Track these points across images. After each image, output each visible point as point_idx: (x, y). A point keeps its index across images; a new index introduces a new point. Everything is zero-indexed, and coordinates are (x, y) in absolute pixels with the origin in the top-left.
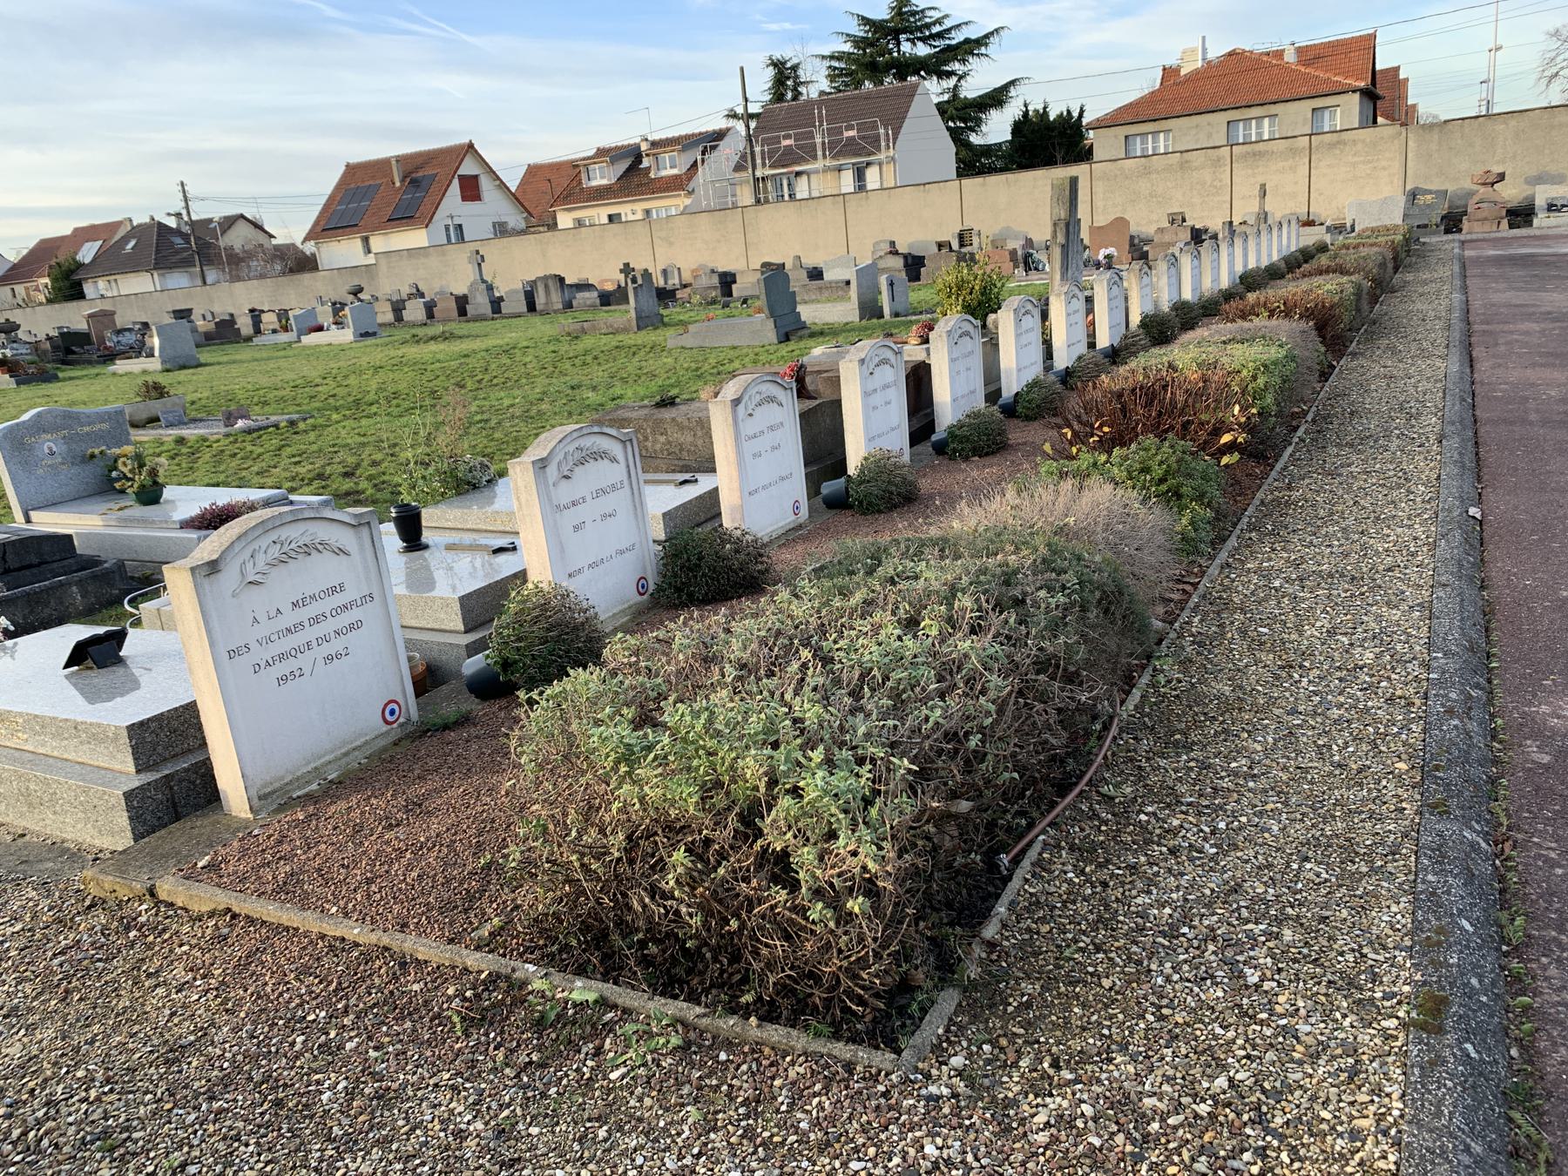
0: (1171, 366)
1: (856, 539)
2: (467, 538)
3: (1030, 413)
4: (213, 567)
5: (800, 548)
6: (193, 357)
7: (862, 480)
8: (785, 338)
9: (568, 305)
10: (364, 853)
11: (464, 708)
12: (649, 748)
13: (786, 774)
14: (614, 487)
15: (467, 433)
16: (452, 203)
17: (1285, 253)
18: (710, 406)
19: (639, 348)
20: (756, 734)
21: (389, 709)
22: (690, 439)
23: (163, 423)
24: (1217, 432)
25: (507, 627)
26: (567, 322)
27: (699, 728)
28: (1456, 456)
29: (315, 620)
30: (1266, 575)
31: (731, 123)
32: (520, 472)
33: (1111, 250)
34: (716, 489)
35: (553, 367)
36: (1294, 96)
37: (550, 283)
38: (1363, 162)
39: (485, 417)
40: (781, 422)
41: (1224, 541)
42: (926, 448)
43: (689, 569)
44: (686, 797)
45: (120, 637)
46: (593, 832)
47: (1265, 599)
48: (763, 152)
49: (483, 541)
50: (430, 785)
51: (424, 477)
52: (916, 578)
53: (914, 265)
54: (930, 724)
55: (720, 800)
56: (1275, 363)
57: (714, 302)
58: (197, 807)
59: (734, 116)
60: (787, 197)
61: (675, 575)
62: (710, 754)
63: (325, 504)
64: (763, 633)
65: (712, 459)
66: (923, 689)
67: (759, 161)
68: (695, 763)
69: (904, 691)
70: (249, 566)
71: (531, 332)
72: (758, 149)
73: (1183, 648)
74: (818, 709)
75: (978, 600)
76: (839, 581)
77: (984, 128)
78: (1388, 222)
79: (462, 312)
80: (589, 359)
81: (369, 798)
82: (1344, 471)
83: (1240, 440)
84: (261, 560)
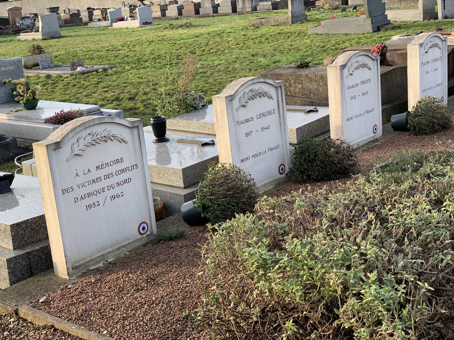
1: (409, 150)
2: (190, 137)
4: (57, 145)
5: (375, 153)
7: (417, 114)
8: (377, 29)
9: (254, 9)
10: (123, 303)
11: (181, 229)
12: (277, 262)
13: (354, 285)
14: (269, 113)
15: (194, 79)
18: (328, 69)
19: (291, 33)
20: (338, 260)
21: (142, 227)
22: (315, 86)
23: (40, 67)
25: (206, 187)
26: (253, 18)
27: (304, 253)
29: (107, 177)
32: (218, 103)
34: (328, 116)
35: (243, 44)
39: (204, 70)
40: (370, 78)
43: (309, 161)
44: (296, 293)
45: (10, 178)
46: (243, 305)
49: (199, 139)
50: (160, 269)
51: (169, 102)
52: (444, 175)
54: (444, 264)
55: (314, 295)
57: (337, 8)
58: (42, 270)
61: (301, 164)
62: (311, 269)
63: (118, 115)
64: (347, 202)
65: (327, 99)
66: (442, 242)
68: (301, 273)
69: (430, 242)
70: (76, 146)
71: (233, 24)
74: (375, 249)
76: (395, 174)
79: (197, 12)
80: (263, 39)
81: (128, 273)
84: (82, 142)
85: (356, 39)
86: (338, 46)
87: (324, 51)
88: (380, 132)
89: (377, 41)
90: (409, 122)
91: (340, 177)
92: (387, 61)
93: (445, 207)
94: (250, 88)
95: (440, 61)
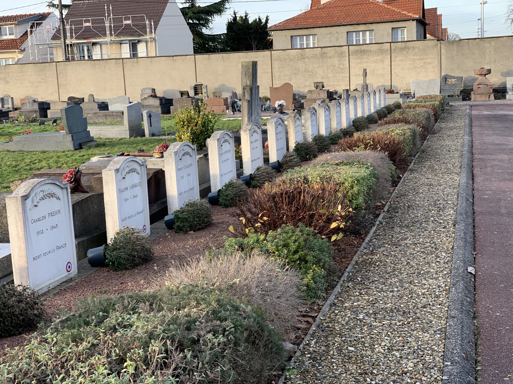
0: (306, 180)
3: (227, 203)
5: (68, 296)
7: (116, 247)
8: (79, 147)
17: (378, 108)
24: (329, 221)
28: (462, 234)
30: (355, 310)
31: (52, 10)
33: (282, 102)
36: (382, 20)
38: (419, 59)
41: (333, 288)
42: (161, 224)
47: (354, 328)
48: (71, 29)
53: (166, 105)
56: (363, 179)
57: (34, 121)
59: (54, 6)
60: (86, 58)
67: (68, 34)
72: (68, 27)
73: (303, 362)
75: (165, 344)
77: (210, 25)
78: (432, 93)
82: (403, 243)
83: (342, 226)
85: (55, 158)
86: (33, 166)
87: (17, 171)
88: (74, 270)
89: (78, 160)
90: (107, 256)
91: (23, 330)
92: (82, 187)
93: (126, 367)
95: (139, 187)
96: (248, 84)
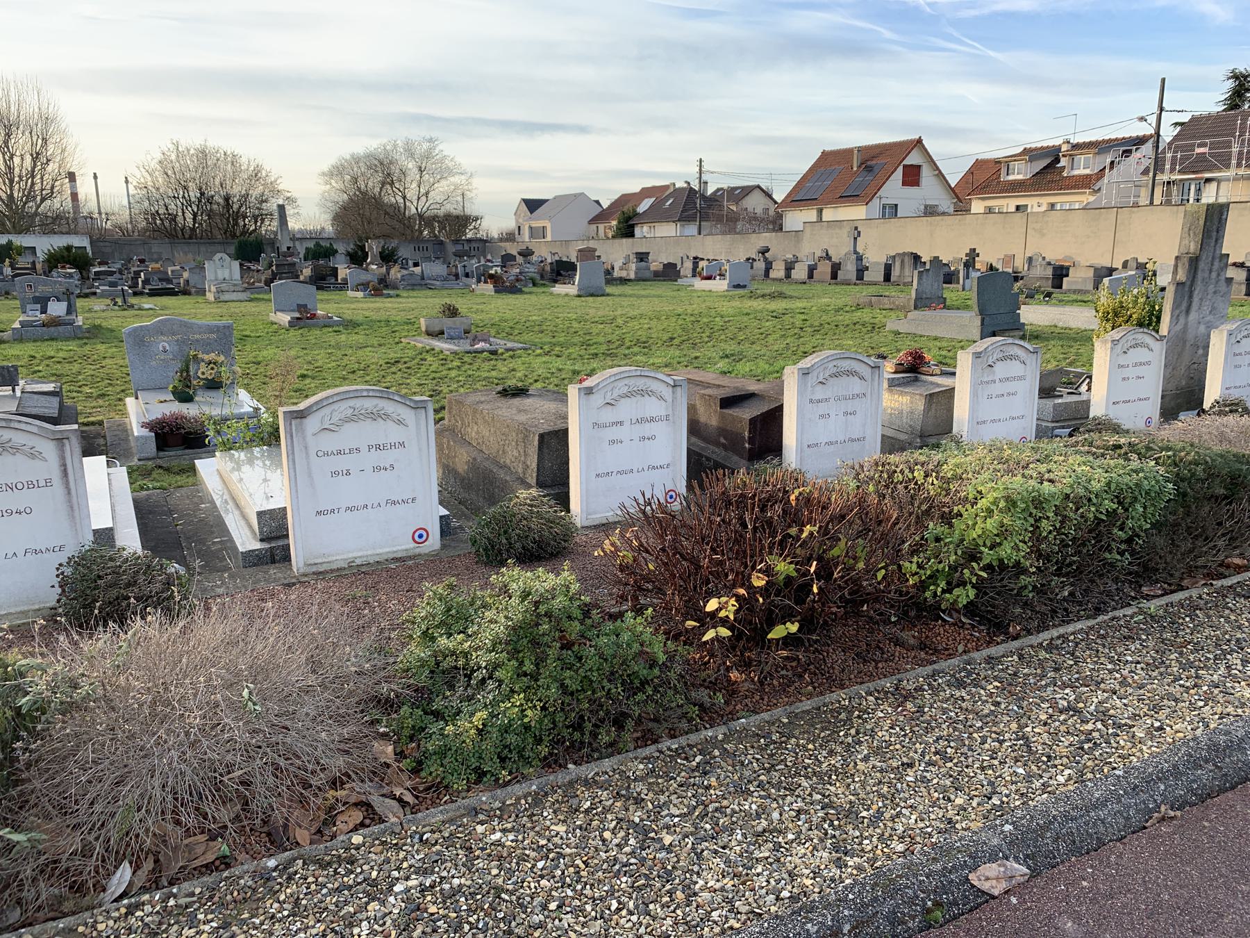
6: (601, 288)
16: (894, 189)
37: (906, 259)
79: (834, 276)
94: (835, 363)
96: (1192, 248)
